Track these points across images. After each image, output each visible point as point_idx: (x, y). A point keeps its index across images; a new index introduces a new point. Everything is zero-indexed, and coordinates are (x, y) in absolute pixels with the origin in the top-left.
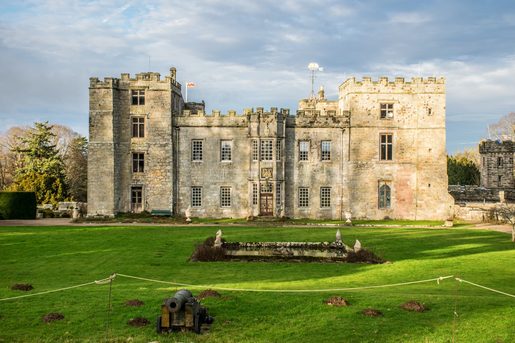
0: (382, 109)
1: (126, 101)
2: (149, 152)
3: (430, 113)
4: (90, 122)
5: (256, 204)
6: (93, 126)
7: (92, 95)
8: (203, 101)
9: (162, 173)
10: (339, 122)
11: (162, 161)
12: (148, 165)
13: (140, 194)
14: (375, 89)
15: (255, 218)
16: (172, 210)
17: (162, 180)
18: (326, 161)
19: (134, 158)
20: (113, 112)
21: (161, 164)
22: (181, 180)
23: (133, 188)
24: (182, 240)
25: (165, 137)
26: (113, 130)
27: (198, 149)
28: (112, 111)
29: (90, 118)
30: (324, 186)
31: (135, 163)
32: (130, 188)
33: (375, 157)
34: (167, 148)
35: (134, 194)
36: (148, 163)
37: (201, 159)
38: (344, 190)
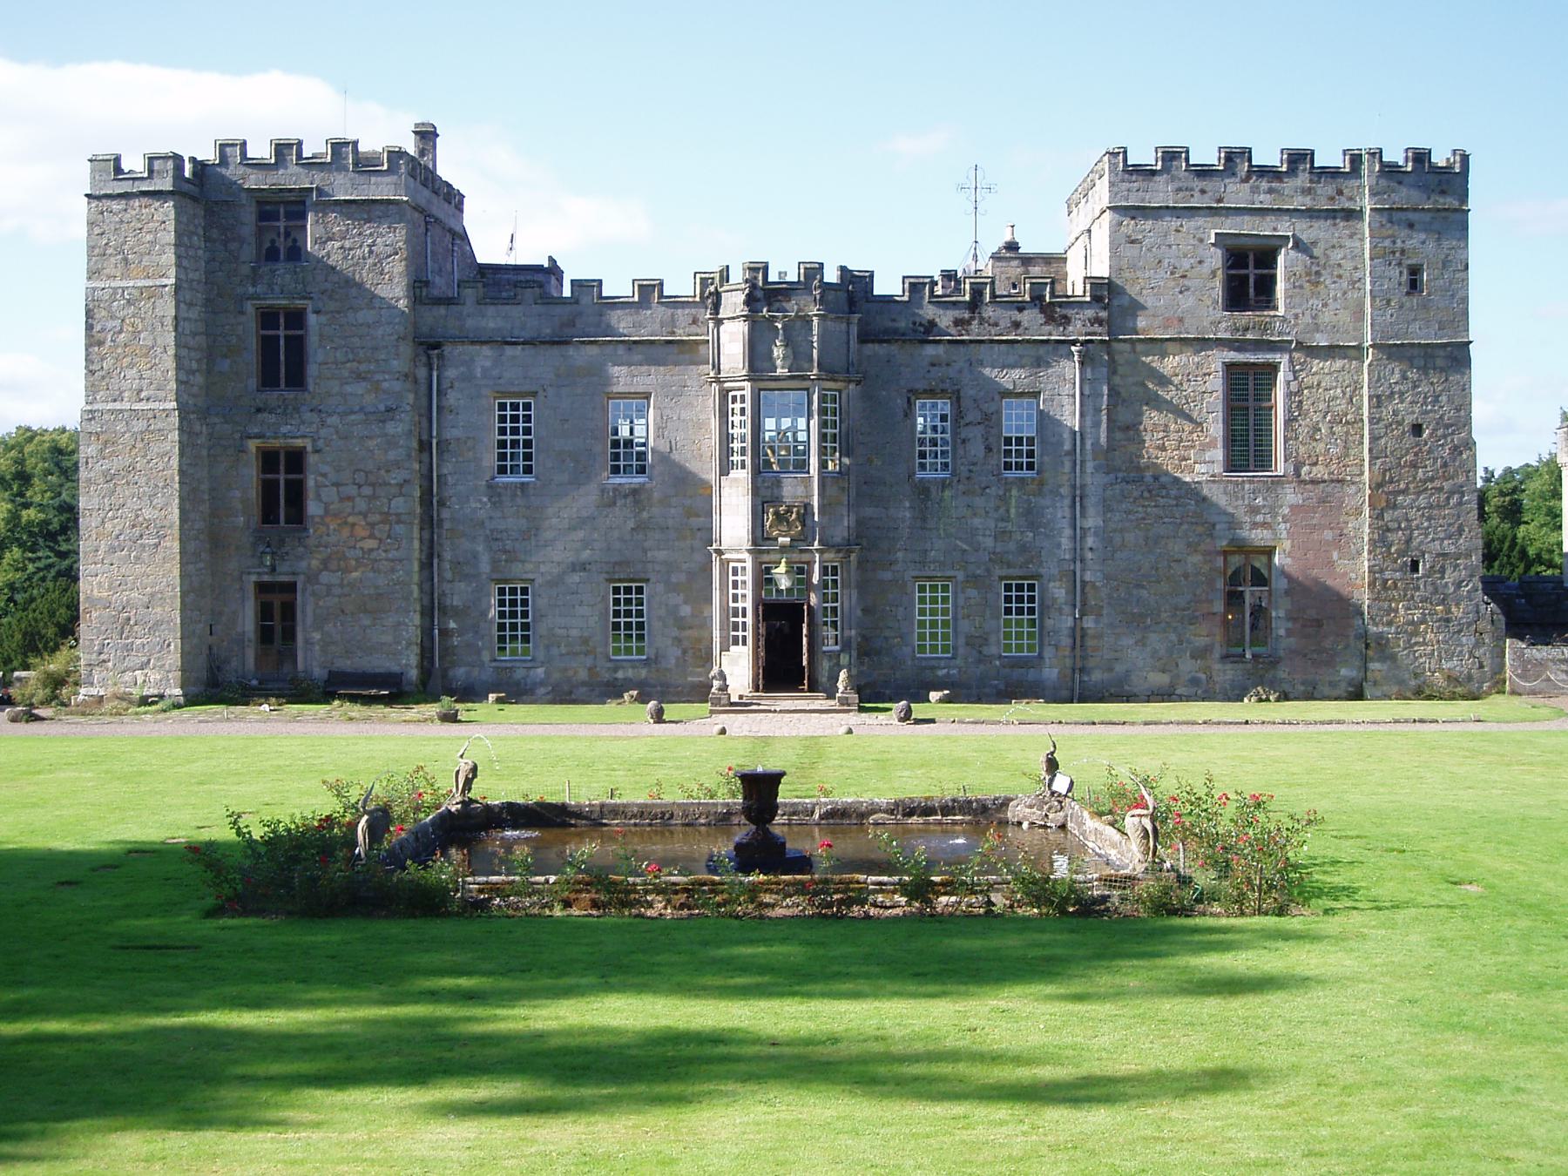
0: (1251, 257)
1: (233, 246)
2: (320, 443)
3: (1414, 286)
4: (89, 327)
5: (744, 643)
6: (100, 343)
7: (1266, 914)
8: (551, 259)
9: (372, 525)
10: (1066, 320)
11: (372, 478)
12: (318, 497)
13: (289, 611)
14: (1203, 192)
15: (990, 420)
16: (414, 674)
17: (374, 555)
18: (1019, 474)
19: (264, 471)
20: (178, 288)
21: (367, 491)
22: (447, 555)
23: (262, 588)
24: (1059, 513)
25: (386, 385)
26: (178, 357)
27: (515, 431)
28: (173, 281)
29: (89, 314)
30: (1012, 572)
31: (269, 491)
32: (251, 589)
33: (1208, 456)
34: (391, 428)
35: (265, 612)
36: (318, 486)
37: (528, 470)
38: (1088, 589)
